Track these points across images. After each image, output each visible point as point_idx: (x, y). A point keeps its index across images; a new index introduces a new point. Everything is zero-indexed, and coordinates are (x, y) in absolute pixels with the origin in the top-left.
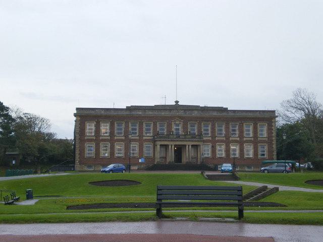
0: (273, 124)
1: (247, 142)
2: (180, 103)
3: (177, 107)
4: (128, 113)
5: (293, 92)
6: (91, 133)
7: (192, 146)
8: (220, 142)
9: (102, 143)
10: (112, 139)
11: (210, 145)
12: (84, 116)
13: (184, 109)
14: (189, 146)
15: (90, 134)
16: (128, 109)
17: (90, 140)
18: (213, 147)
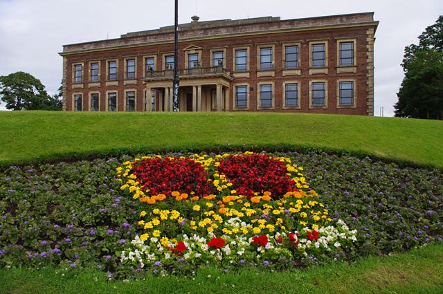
0: (369, 39)
4: (122, 44)
7: (203, 87)
8: (265, 80)
11: (172, 77)
12: (75, 56)
13: (204, 27)
16: (125, 38)
18: (251, 89)
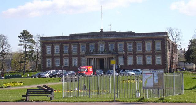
1: (148, 54)
2: (103, 31)
3: (102, 33)
5: (8, 37)
6: (49, 52)
9: (56, 58)
10: (61, 56)
14: (105, 58)
15: (49, 53)
17: (57, 57)
